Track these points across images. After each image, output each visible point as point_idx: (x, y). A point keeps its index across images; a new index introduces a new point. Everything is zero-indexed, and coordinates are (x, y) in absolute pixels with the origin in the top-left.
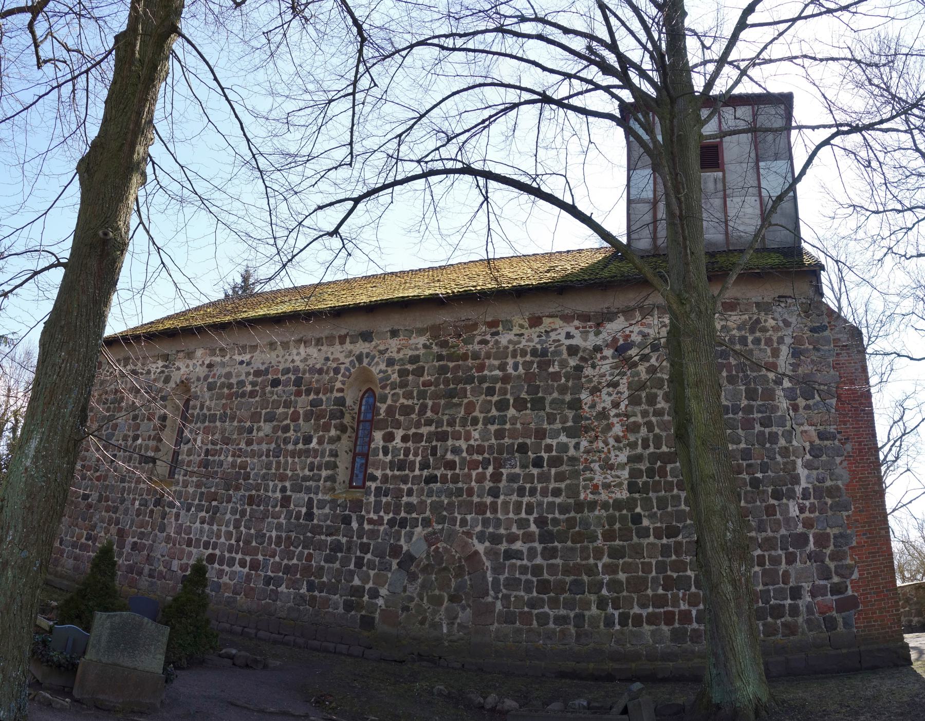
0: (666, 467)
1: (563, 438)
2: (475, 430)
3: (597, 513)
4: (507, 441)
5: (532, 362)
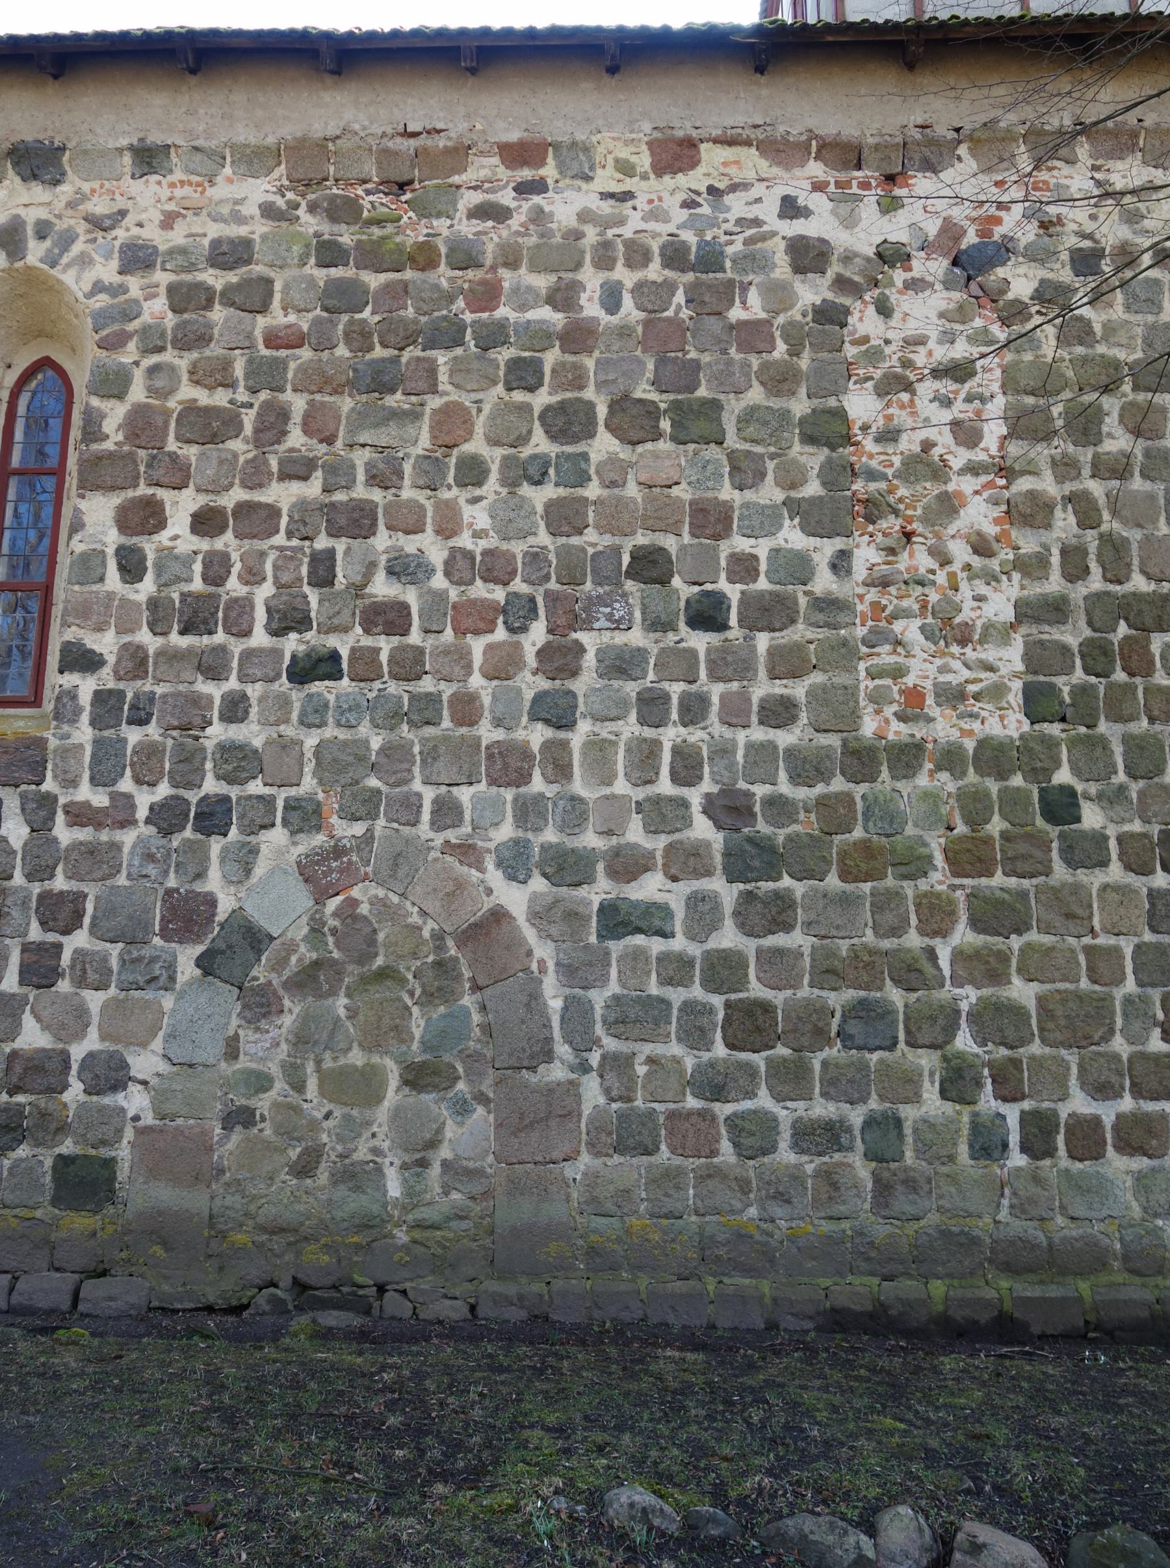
0: (1148, 641)
1: (792, 536)
2: (475, 500)
3: (922, 780)
4: (592, 539)
5: (669, 287)
